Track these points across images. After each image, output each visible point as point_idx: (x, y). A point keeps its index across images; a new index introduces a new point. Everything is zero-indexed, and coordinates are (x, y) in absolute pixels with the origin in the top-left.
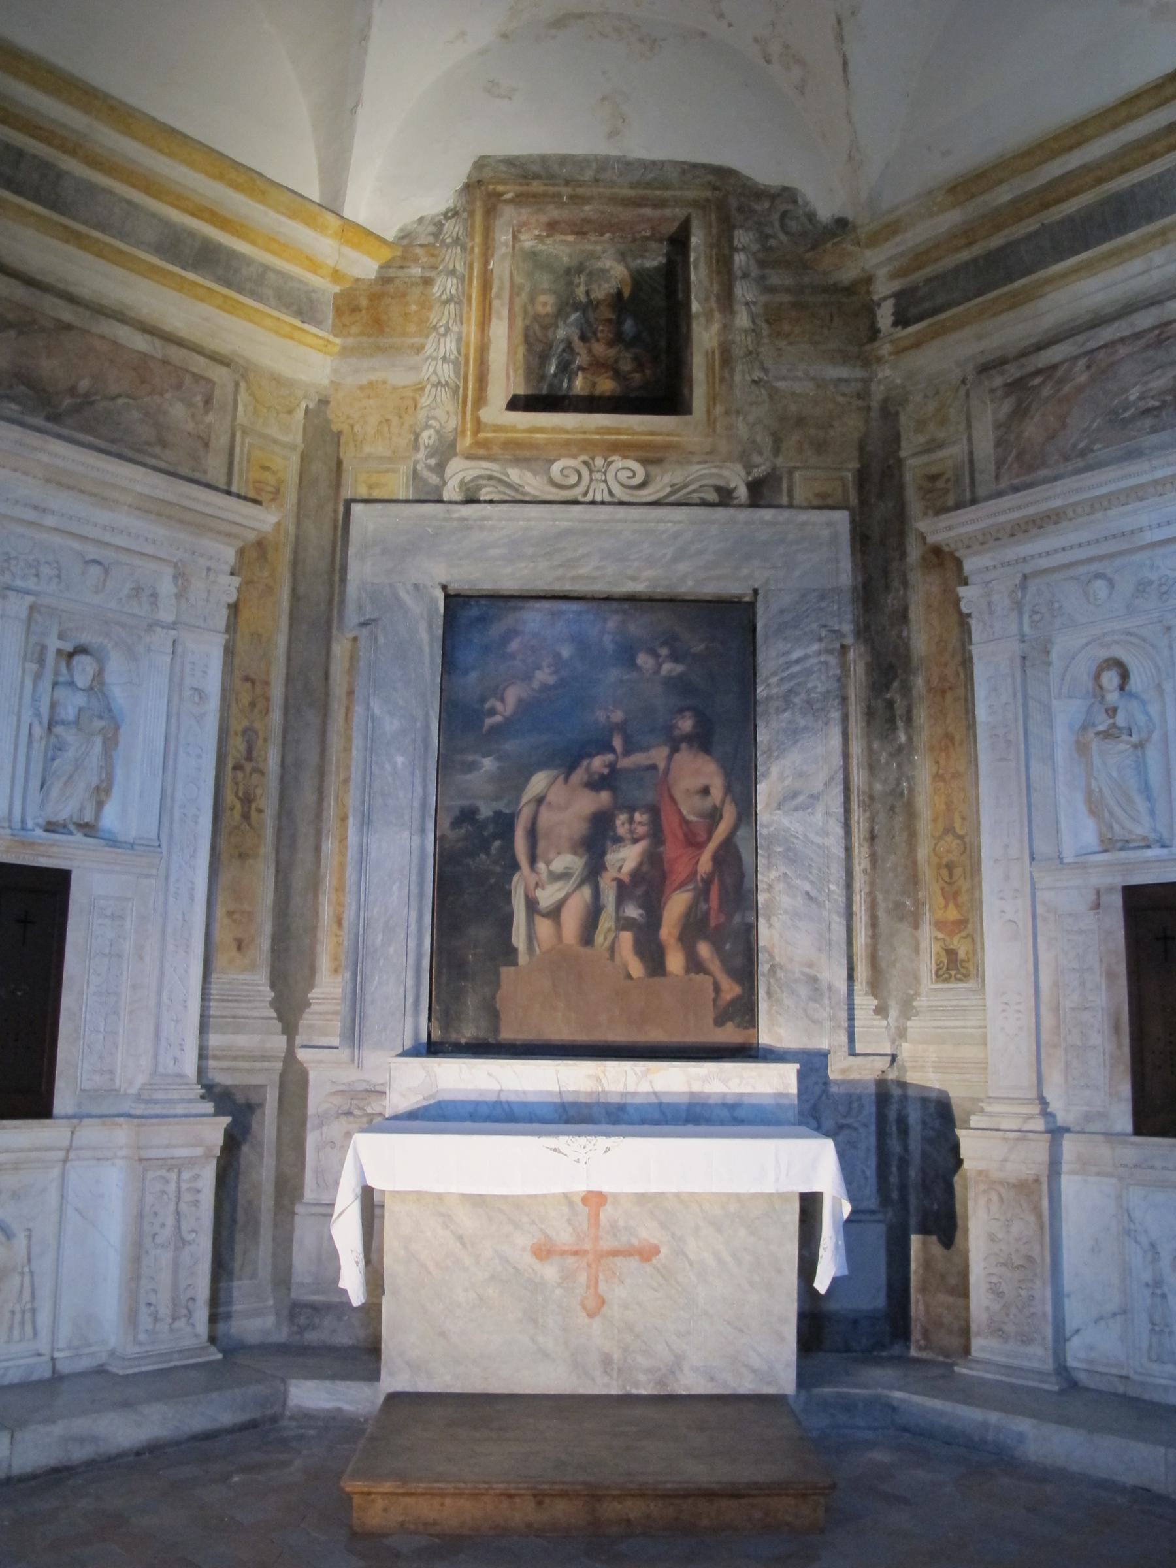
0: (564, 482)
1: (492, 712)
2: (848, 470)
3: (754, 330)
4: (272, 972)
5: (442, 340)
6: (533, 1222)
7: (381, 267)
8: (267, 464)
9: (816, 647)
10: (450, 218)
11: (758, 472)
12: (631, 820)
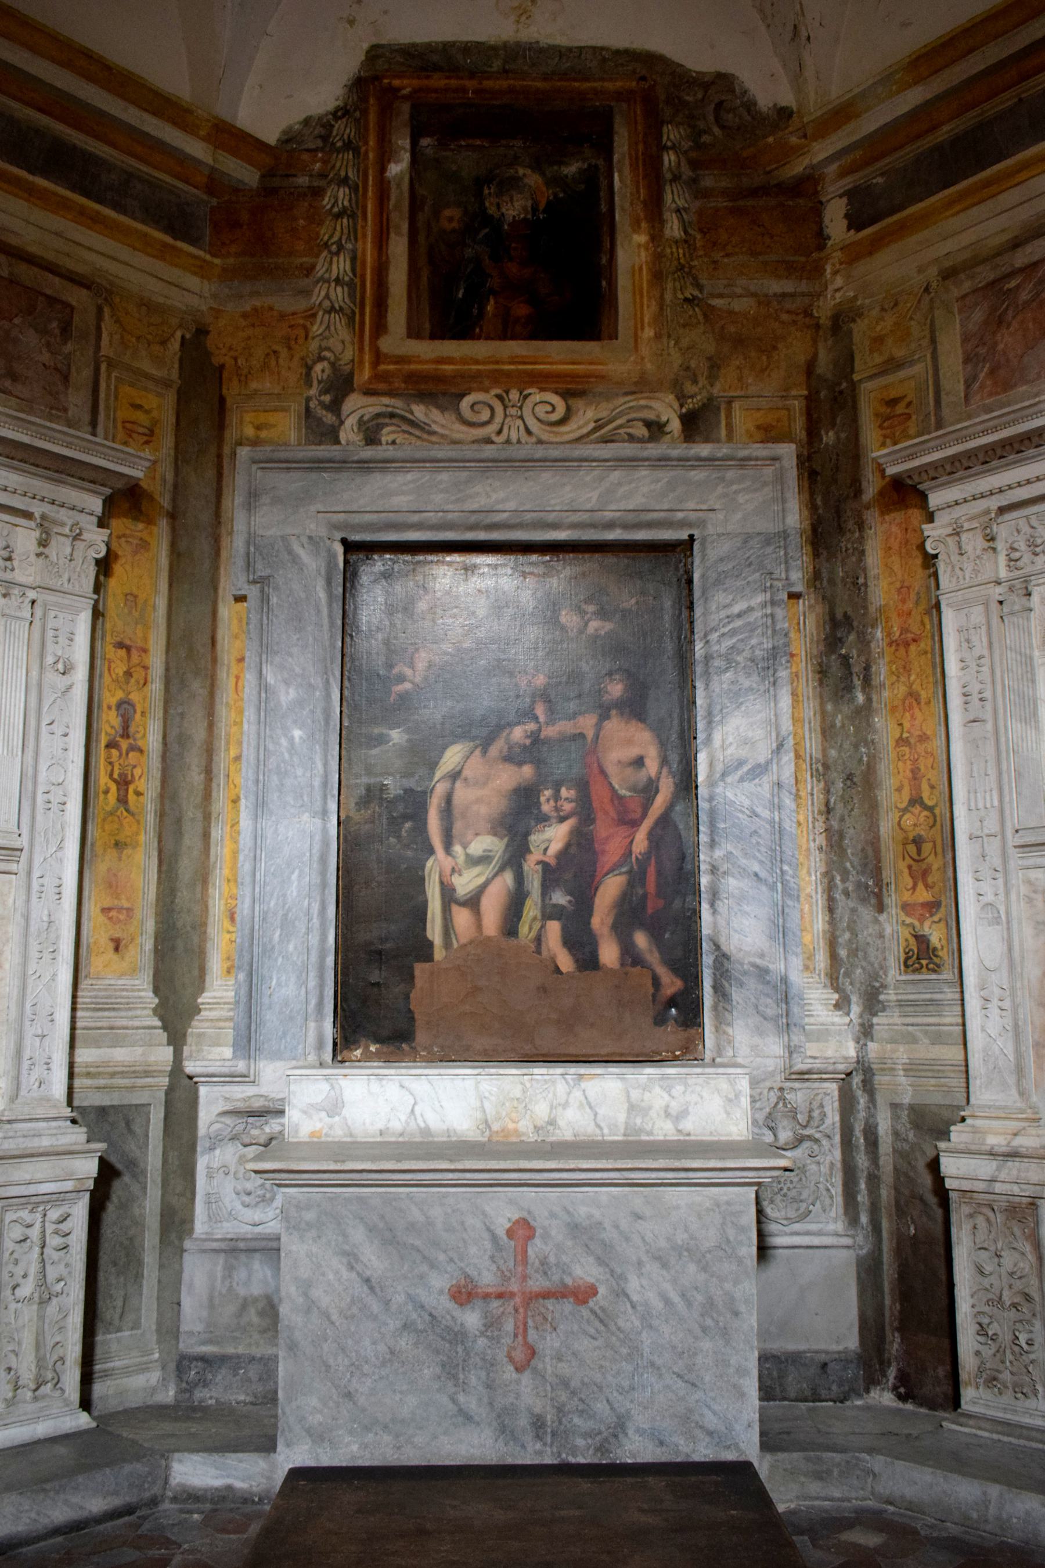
0: (473, 418)
1: (401, 679)
2: (795, 397)
3: (686, 241)
4: (155, 975)
5: (335, 259)
6: (451, 1260)
7: (263, 176)
8: (138, 402)
9: (760, 598)
10: (341, 118)
11: (690, 404)
12: (557, 797)
